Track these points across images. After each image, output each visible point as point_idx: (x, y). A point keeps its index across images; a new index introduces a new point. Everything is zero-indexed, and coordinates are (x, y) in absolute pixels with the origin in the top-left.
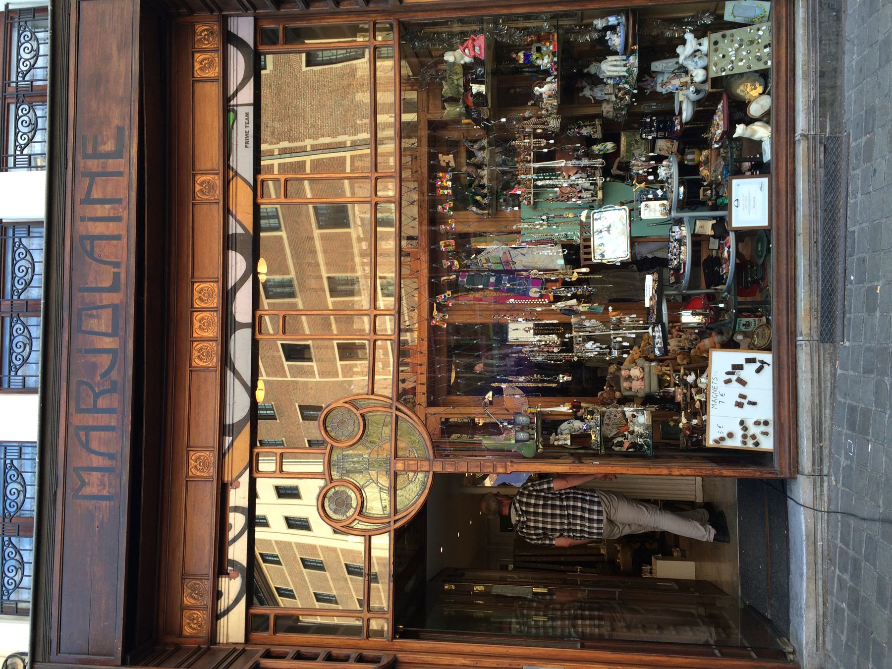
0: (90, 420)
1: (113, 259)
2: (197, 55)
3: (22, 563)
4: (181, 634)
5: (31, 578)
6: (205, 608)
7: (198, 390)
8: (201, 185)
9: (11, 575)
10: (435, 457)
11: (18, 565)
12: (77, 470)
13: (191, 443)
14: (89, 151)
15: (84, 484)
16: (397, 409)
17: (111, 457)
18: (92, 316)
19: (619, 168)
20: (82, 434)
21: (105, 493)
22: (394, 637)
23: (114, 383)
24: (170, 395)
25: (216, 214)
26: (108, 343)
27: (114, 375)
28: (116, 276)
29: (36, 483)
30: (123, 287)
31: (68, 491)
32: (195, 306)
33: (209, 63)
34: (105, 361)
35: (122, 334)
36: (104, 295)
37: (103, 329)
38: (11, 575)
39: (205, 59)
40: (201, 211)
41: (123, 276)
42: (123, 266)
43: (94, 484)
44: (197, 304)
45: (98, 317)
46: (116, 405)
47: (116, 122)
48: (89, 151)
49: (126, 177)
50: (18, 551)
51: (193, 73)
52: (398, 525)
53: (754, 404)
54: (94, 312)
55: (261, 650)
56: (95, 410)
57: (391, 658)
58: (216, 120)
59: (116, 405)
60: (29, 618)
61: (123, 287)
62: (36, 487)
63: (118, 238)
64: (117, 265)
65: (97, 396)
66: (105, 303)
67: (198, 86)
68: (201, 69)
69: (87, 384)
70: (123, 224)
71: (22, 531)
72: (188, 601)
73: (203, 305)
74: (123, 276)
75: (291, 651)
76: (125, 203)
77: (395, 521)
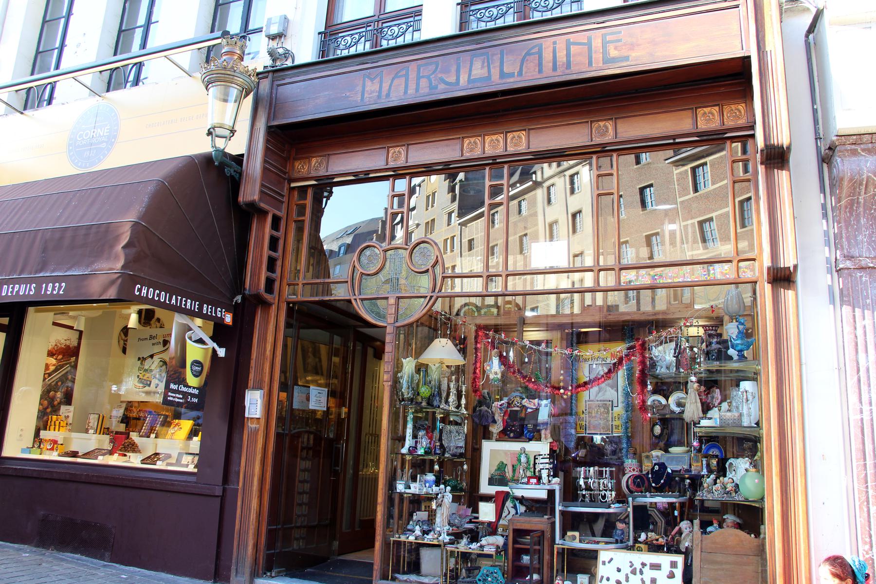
0: (412, 75)
1: (524, 70)
2: (717, 108)
3: (496, 19)
4: (296, 159)
5: (485, 28)
6: (309, 172)
7: (447, 146)
8: (710, 113)
9: (487, 14)
10: (398, 327)
11: (549, 7)
13: (531, 132)
14: (608, 38)
15: (372, 80)
16: (431, 297)
17: (388, 95)
18: (483, 62)
19: (491, 482)
20: (404, 72)
21: (366, 95)
22: (288, 303)
24: (551, 113)
25: (580, 141)
26: (463, 79)
28: (512, 75)
29: (564, 14)
30: (504, 81)
31: (368, 71)
32: (486, 137)
33: (710, 119)
34: (452, 79)
35: (470, 86)
36: (498, 69)
37: (474, 72)
38: (487, 14)
39: (740, 112)
40: (456, 145)
41: (512, 80)
42: (519, 79)
43: (371, 87)
44: (488, 139)
45: (483, 67)
46: (421, 91)
47: (634, 54)
49: (588, 69)
50: (503, 15)
51: (700, 107)
52: (353, 302)
53: (612, 559)
54: (486, 64)
55: (282, 214)
56: (419, 78)
57: (272, 301)
58: (660, 131)
59: (421, 91)
60: (458, 33)
61: (504, 81)
62: (560, 15)
63: (540, 71)
64: (520, 73)
65: (428, 77)
66: (492, 71)
67: (688, 113)
68: (705, 113)
69: (437, 68)
70: (551, 73)
71: (522, 12)
72: (314, 161)
73: (509, 140)
74: (512, 80)
75: (280, 234)
76: (567, 71)
77: (356, 299)
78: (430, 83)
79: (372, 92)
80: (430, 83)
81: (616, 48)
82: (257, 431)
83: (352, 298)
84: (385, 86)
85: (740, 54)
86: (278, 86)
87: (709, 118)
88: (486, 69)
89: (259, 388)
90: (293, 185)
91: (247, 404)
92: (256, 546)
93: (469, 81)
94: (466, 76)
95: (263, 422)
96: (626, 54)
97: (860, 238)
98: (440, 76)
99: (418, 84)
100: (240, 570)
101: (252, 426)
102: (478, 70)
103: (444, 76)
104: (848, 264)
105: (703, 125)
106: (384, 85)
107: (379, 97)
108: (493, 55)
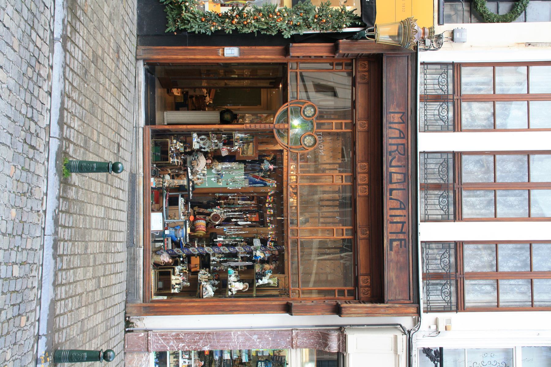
12: (404, 123)
14: (403, 242)
15: (401, 118)
17: (390, 128)
18: (400, 180)
20: (402, 136)
21: (392, 115)
23: (390, 155)
26: (393, 170)
27: (390, 158)
28: (391, 194)
37: (395, 175)
42: (388, 198)
45: (397, 179)
46: (389, 147)
48: (403, 242)
52: (286, 104)
54: (399, 181)
56: (398, 145)
61: (388, 191)
63: (391, 209)
64: (391, 199)
66: (395, 185)
74: (388, 195)
78: (393, 152)
79: (393, 118)
80: (393, 152)
81: (397, 245)
82: (217, 54)
83: (288, 103)
84: (396, 126)
85: (386, 299)
86: (408, 57)
87: (363, 281)
88: (396, 181)
89: (240, 54)
90: (354, 61)
91: (232, 48)
92: (159, 59)
93: (391, 173)
94: (394, 171)
95: (223, 57)
96: (393, 249)
97: (305, 339)
98: (397, 157)
99: (394, 144)
100: (146, 51)
101: (220, 52)
102: (396, 177)
103: (396, 159)
104: (294, 334)
105: (361, 278)
106: (397, 125)
107: (390, 123)
108: (403, 185)
